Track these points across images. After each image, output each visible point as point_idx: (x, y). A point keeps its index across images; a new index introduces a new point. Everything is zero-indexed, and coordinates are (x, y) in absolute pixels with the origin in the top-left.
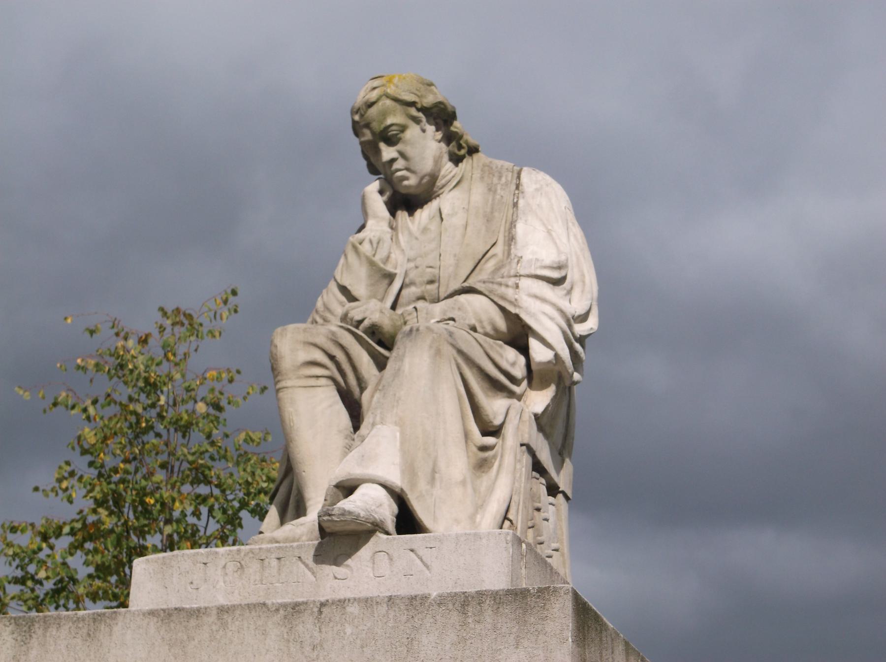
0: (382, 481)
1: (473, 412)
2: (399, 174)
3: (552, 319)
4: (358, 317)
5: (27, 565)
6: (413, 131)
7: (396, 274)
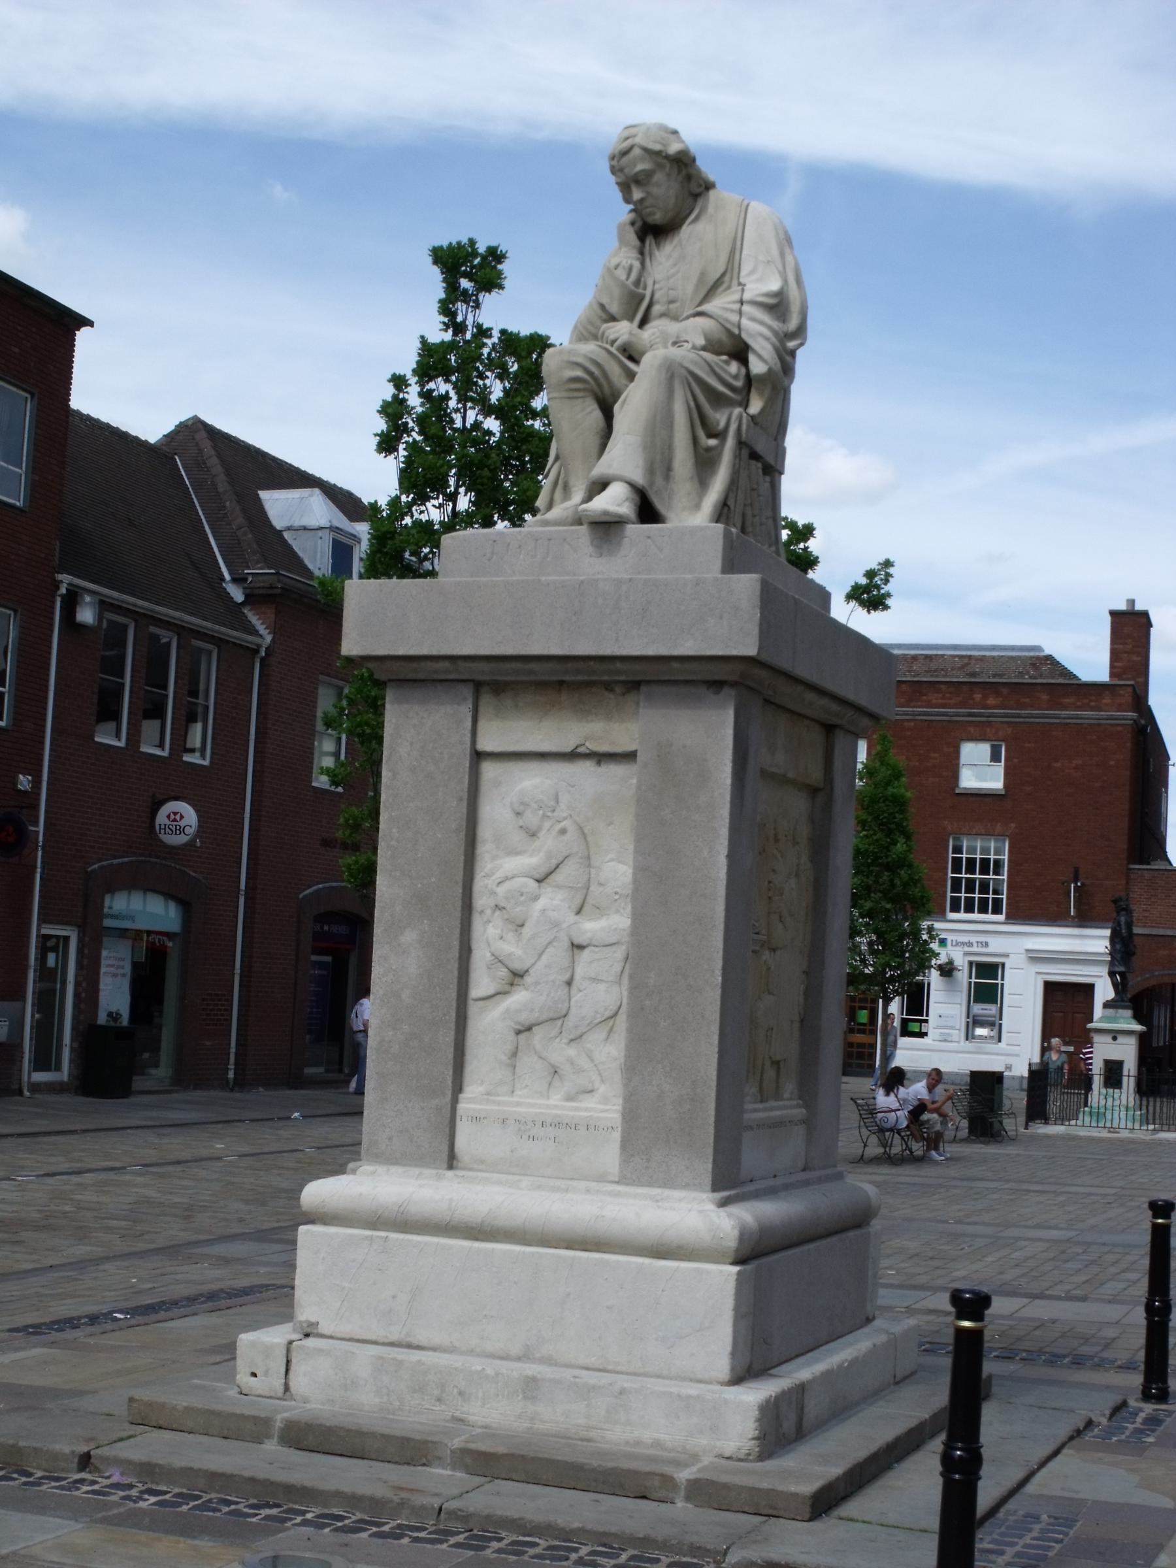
2: (648, 210)
3: (767, 339)
4: (612, 337)
6: (659, 177)
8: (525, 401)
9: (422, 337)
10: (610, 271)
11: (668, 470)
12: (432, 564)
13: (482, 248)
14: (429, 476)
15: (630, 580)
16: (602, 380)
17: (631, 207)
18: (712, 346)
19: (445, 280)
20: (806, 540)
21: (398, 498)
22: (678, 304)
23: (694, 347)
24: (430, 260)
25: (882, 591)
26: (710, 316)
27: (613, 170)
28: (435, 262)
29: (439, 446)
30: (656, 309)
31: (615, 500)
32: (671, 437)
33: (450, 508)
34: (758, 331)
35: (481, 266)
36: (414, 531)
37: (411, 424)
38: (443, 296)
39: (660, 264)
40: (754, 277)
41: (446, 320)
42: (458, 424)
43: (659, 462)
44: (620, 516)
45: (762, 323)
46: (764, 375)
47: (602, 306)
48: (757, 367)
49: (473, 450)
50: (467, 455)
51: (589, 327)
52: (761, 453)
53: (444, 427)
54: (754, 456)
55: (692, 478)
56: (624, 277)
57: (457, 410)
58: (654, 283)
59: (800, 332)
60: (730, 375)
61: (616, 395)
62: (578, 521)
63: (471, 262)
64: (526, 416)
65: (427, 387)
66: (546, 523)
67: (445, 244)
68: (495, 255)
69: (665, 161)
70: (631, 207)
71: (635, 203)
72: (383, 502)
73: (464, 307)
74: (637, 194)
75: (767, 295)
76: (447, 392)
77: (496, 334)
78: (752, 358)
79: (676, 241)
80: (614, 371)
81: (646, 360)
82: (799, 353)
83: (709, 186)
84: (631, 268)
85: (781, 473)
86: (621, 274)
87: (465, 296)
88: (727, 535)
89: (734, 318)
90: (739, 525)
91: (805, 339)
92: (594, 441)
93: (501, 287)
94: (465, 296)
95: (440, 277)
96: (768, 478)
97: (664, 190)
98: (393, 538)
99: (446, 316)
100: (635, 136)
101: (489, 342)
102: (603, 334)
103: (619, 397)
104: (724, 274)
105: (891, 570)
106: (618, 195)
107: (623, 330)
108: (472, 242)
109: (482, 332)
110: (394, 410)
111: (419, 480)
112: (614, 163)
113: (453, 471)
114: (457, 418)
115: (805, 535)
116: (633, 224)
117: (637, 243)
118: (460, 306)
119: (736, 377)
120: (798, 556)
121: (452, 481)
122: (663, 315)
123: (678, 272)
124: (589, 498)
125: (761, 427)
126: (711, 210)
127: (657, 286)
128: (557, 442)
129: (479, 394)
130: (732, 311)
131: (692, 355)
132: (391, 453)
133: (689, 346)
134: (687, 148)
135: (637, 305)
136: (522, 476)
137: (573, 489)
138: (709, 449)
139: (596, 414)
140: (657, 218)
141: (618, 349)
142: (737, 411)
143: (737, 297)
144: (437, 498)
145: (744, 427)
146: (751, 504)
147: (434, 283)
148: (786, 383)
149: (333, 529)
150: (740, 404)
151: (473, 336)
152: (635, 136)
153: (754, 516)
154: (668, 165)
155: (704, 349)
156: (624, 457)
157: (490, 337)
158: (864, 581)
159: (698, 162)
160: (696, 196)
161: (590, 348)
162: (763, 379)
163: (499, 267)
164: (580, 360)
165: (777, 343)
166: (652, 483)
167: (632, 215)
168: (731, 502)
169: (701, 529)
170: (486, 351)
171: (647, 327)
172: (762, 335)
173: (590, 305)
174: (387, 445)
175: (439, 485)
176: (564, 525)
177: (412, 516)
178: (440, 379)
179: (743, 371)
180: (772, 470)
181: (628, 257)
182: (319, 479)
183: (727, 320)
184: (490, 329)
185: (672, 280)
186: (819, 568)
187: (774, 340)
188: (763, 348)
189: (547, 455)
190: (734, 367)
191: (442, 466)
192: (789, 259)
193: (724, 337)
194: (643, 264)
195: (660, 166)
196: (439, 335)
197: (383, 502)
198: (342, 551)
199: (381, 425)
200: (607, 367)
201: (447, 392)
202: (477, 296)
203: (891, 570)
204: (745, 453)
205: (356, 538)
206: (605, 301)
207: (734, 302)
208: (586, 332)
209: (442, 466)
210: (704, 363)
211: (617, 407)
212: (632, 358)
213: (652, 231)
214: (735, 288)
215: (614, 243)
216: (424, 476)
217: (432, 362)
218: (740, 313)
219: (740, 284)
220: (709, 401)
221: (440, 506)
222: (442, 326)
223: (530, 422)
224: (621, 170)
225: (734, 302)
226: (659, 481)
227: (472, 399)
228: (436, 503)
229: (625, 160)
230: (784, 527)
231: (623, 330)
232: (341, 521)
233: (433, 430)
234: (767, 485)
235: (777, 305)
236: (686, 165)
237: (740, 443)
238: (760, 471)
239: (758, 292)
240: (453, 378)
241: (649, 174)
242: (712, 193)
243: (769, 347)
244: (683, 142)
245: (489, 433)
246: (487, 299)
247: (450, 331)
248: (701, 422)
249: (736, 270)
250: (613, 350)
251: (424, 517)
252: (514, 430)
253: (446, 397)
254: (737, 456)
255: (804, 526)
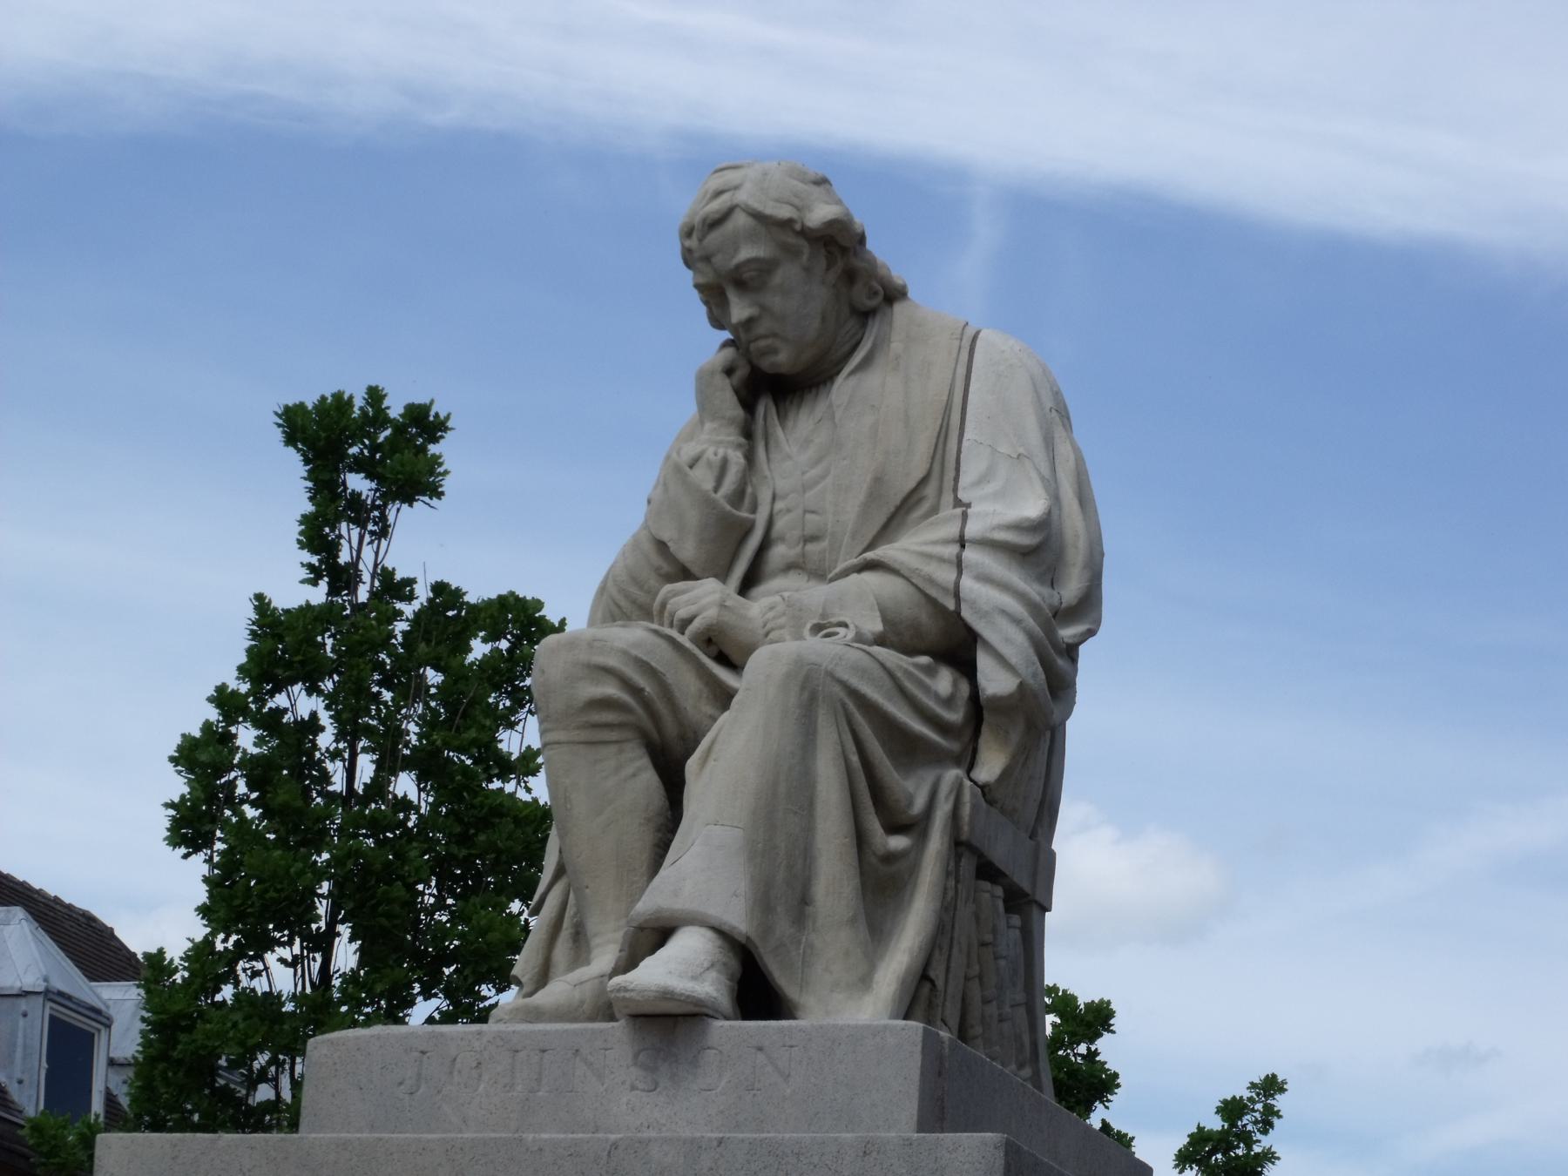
0: (716, 924)
1: (875, 804)
2: (762, 343)
3: (1017, 621)
4: (682, 613)
5: (213, 934)
6: (787, 273)
7: (735, 691)
8: (484, 737)
9: (259, 597)
10: (678, 472)
11: (803, 901)
12: (276, 1088)
13: (395, 408)
14: (272, 894)
15: (720, 1142)
16: (661, 707)
17: (726, 335)
18: (897, 636)
19: (311, 476)
20: (1093, 1037)
21: (208, 943)
22: (824, 544)
23: (859, 638)
24: (278, 435)
25: (1257, 1149)
26: (895, 572)
27: (689, 259)
28: (290, 440)
29: (295, 830)
30: (779, 553)
31: (684, 967)
32: (809, 829)
33: (316, 967)
34: (995, 602)
35: (393, 446)
36: (237, 1017)
37: (241, 788)
38: (309, 508)
39: (789, 457)
40: (989, 488)
41: (315, 560)
42: (338, 784)
43: (783, 884)
44: (698, 1002)
45: (1004, 587)
46: (1011, 696)
47: (662, 546)
48: (995, 681)
49: (370, 842)
50: (357, 853)
51: (633, 590)
52: (1002, 867)
53: (307, 790)
54: (988, 871)
55: (853, 921)
56: (709, 485)
57: (335, 755)
58: (774, 498)
59: (1087, 606)
60: (937, 697)
61: (690, 740)
62: (605, 1010)
63: (373, 438)
64: (487, 769)
65: (271, 704)
66: (536, 1015)
67: (310, 402)
68: (424, 424)
69: (802, 242)
70: (726, 335)
71: (734, 329)
72: (176, 951)
73: (355, 532)
74: (739, 310)
75: (1017, 527)
76: (314, 715)
77: (423, 594)
78: (984, 662)
79: (821, 407)
80: (686, 685)
81: (757, 663)
82: (1084, 650)
83: (893, 295)
84: (724, 466)
85: (1046, 908)
86: (703, 478)
87: (357, 511)
88: (930, 1044)
89: (946, 575)
90: (954, 1022)
91: (1098, 622)
92: (639, 839)
93: (436, 493)
94: (357, 511)
95: (302, 470)
96: (1016, 920)
97: (797, 298)
98: (190, 1029)
99: (314, 551)
100: (736, 188)
101: (408, 609)
102: (663, 605)
103: (697, 743)
104: (924, 481)
105: (1280, 1102)
106: (698, 310)
107: (705, 598)
108: (375, 396)
109: (393, 587)
110: (201, 756)
111: (249, 905)
112: (692, 243)
113: (325, 887)
114: (336, 770)
115: (1089, 1025)
116: (729, 371)
117: (739, 412)
118: (348, 533)
119: (948, 702)
120: (1073, 1071)
121: (322, 908)
122: (790, 567)
123: (823, 477)
124: (630, 962)
125: (1003, 811)
126: (896, 346)
127: (779, 505)
128: (562, 837)
129: (382, 721)
130: (942, 560)
131: (855, 655)
132: (197, 850)
133: (851, 634)
134: (848, 214)
135: (737, 543)
136: (475, 900)
137: (595, 942)
138: (890, 858)
139: (648, 779)
140: (782, 359)
141: (694, 640)
142: (952, 774)
143: (952, 530)
144: (290, 943)
145: (966, 810)
146: (980, 977)
147: (287, 486)
148: (1056, 717)
149: (50, 995)
150: (957, 761)
151: (373, 594)
152: (736, 188)
153: (986, 1001)
154: (806, 250)
155: (880, 641)
156: (706, 874)
157: (410, 598)
158: (1215, 1124)
159: (870, 245)
160: (865, 316)
161: (633, 636)
162: (1007, 707)
163: (433, 449)
164: (612, 662)
165: (1037, 630)
166: (767, 930)
167: (730, 352)
168: (937, 973)
169: (876, 1031)
170: (401, 627)
171: (757, 591)
172: (1003, 612)
173: (635, 543)
174: (189, 828)
175: (295, 916)
176: (575, 1020)
177: (237, 983)
178: (297, 688)
179: (965, 688)
180: (1025, 899)
181: (720, 443)
182: (24, 885)
183: (931, 581)
184: (410, 582)
185: (809, 494)
186: (1117, 1099)
187: (1031, 622)
188: (1007, 640)
189: (536, 859)
190: (944, 681)
191: (301, 873)
192: (1063, 449)
193: (925, 617)
194: (750, 457)
195: (791, 252)
196: (295, 590)
197: (176, 951)
198: (71, 1042)
199: (177, 786)
200: (670, 678)
201: (314, 715)
202: (382, 509)
203: (1280, 1102)
204: (968, 865)
205: (101, 1018)
206: (666, 536)
207: (946, 542)
208: (624, 600)
209: (301, 873)
210: (878, 672)
211: (691, 764)
212: (723, 659)
213: (767, 387)
214: (948, 511)
215: (687, 408)
216: (261, 896)
217: (280, 646)
218: (959, 565)
219: (958, 503)
220: (891, 754)
221: (294, 963)
222: (304, 573)
223: (496, 784)
224: (707, 259)
225: (946, 542)
226: (783, 927)
227: (369, 732)
228: (285, 953)
229: (715, 237)
230: (1050, 1009)
231: (705, 598)
232: (70, 979)
233: (282, 797)
234: (1016, 934)
235: (1038, 549)
236: (844, 250)
237: (959, 845)
238: (1000, 904)
239: (996, 521)
240: (328, 685)
241: (765, 268)
242: (898, 308)
243: (1020, 638)
244: (839, 202)
245: (405, 804)
246: (408, 519)
247: (323, 585)
248: (874, 799)
249: (950, 474)
250: (684, 640)
251: (261, 985)
252: (461, 799)
253: (312, 726)
254: (951, 872)
255: (1089, 1006)
